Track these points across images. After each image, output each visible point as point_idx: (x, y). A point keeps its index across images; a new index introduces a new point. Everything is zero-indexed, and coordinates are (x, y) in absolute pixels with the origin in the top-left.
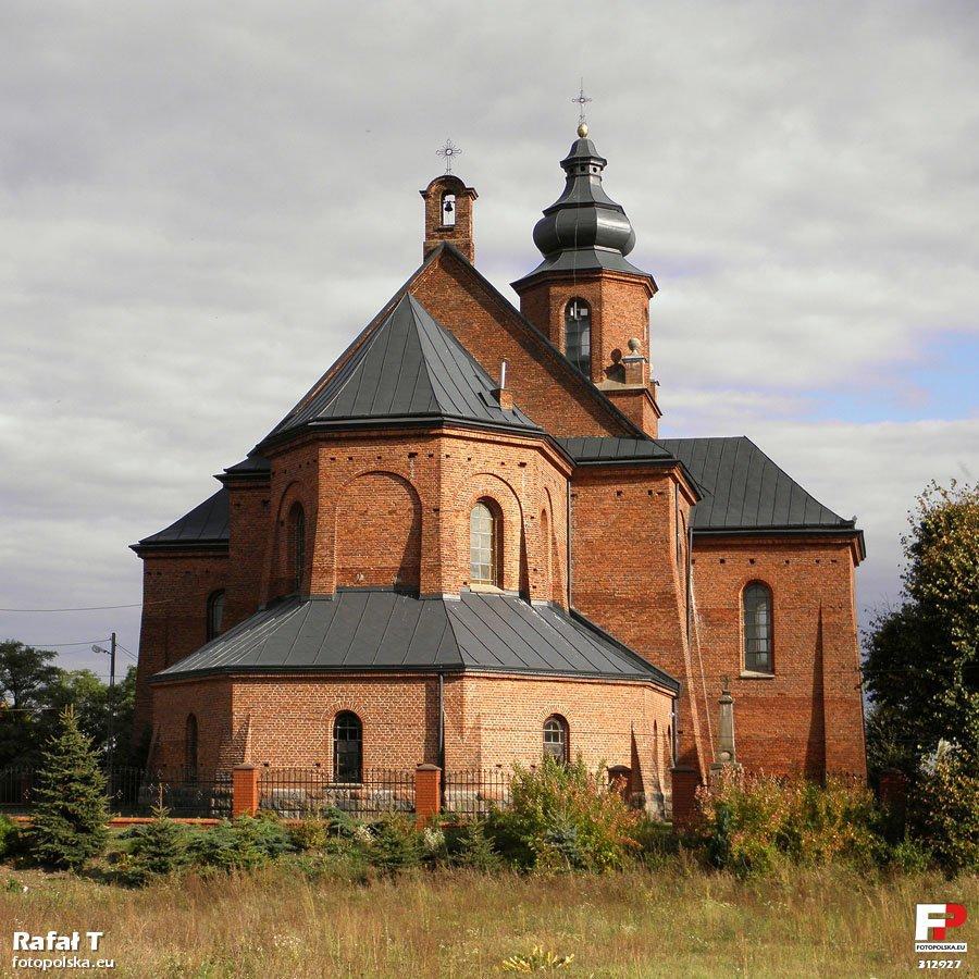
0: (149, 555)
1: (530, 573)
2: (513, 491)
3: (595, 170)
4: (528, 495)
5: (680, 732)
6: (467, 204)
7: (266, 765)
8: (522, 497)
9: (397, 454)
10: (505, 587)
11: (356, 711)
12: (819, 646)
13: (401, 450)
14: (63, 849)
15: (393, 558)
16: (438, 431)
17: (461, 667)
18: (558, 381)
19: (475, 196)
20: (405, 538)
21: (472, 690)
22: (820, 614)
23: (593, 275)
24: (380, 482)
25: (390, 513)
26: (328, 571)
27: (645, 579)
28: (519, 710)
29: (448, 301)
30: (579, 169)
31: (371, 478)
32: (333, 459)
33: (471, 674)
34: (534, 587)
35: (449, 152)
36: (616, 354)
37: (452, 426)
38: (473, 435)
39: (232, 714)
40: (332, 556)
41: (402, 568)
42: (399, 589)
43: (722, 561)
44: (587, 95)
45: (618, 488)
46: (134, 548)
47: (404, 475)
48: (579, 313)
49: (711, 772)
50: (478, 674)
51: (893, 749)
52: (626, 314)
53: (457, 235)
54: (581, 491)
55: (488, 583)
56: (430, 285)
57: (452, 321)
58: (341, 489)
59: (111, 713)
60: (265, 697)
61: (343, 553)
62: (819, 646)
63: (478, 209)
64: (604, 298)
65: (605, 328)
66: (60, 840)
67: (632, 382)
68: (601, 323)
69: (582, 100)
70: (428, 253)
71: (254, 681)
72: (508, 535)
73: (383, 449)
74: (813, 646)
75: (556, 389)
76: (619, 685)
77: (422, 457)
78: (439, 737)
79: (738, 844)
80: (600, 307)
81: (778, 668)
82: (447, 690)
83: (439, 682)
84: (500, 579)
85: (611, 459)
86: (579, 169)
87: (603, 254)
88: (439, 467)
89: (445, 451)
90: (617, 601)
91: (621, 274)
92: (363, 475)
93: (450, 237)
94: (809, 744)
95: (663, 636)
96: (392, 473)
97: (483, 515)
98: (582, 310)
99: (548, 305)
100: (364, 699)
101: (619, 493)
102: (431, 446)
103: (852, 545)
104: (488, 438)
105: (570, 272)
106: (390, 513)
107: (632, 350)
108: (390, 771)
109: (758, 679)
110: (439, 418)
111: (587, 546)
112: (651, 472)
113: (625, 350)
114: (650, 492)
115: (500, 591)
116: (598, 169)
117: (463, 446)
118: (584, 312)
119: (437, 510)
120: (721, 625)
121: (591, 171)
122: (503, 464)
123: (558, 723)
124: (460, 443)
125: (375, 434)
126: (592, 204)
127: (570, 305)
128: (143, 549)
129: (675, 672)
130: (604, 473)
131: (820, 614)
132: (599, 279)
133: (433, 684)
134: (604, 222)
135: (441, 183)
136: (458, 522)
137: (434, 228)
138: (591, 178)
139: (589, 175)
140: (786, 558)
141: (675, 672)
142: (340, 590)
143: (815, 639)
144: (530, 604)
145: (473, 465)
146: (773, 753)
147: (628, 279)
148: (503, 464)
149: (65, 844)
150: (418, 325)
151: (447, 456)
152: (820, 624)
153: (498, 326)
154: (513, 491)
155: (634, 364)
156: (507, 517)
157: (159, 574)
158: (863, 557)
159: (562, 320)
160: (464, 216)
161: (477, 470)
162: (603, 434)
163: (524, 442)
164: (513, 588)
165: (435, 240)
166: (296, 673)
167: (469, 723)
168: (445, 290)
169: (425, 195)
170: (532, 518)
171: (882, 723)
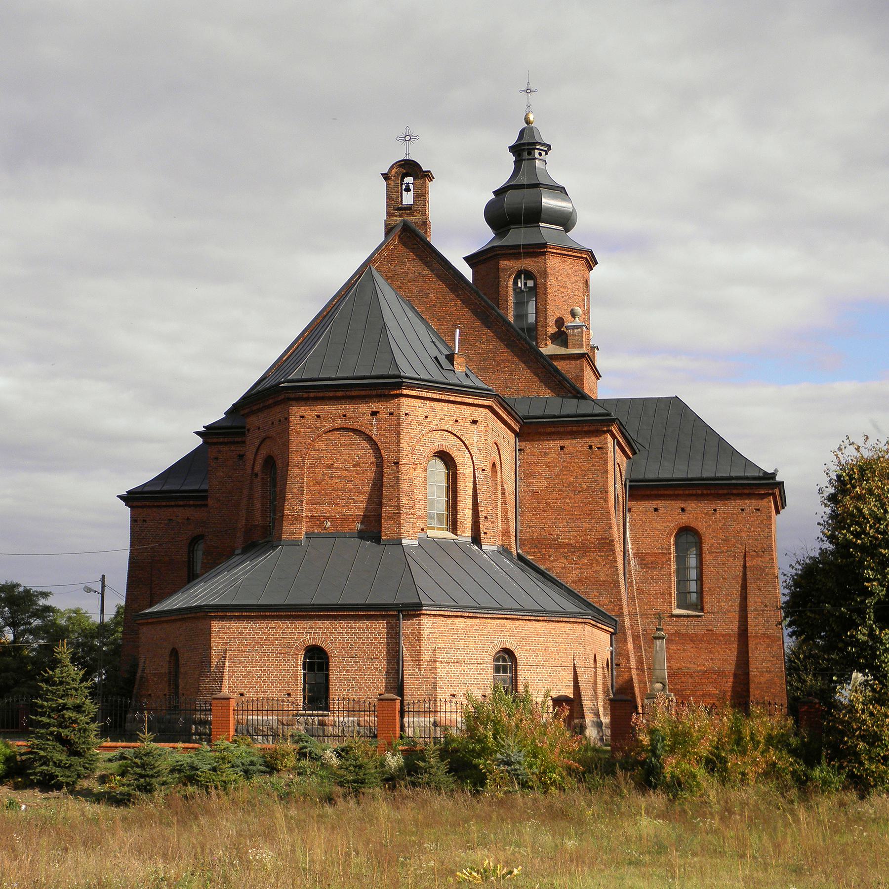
0: (135, 504)
1: (482, 521)
3: (540, 154)
5: (618, 665)
7: (242, 695)
8: (474, 451)
10: (459, 533)
12: (744, 587)
13: (365, 408)
14: (57, 771)
15: (357, 507)
16: (398, 392)
17: (419, 606)
18: (507, 346)
20: (367, 489)
21: (428, 625)
22: (745, 558)
23: (538, 250)
25: (354, 466)
26: (298, 519)
27: (586, 526)
29: (407, 273)
31: (337, 434)
32: (302, 417)
33: (428, 612)
34: (485, 533)
35: (408, 138)
36: (560, 322)
37: (411, 387)
38: (430, 395)
40: (301, 505)
41: (365, 516)
42: (362, 535)
43: (656, 510)
45: (562, 443)
47: (367, 432)
48: (525, 284)
49: (646, 701)
51: (811, 681)
52: (568, 285)
54: (532, 448)
56: (390, 259)
57: (410, 291)
60: (241, 633)
62: (744, 587)
63: (435, 191)
64: (549, 271)
66: (55, 763)
67: (574, 346)
69: (528, 91)
70: (389, 230)
71: (231, 618)
72: (461, 485)
73: (349, 408)
74: (738, 587)
75: (504, 353)
76: (562, 622)
77: (384, 415)
79: (671, 766)
81: (707, 606)
82: (406, 627)
84: (454, 527)
85: (555, 417)
86: (525, 154)
87: (548, 231)
88: (399, 424)
89: (404, 409)
90: (560, 546)
92: (330, 431)
93: (408, 215)
94: (735, 675)
95: (602, 578)
96: (356, 430)
97: (439, 469)
99: (497, 277)
101: (562, 448)
102: (391, 405)
103: (774, 495)
104: (443, 397)
106: (354, 466)
107: (575, 318)
109: (688, 616)
111: (533, 495)
112: (575, 429)
114: (590, 447)
115: (454, 536)
116: (543, 153)
119: (397, 463)
120: (655, 568)
121: (537, 155)
122: (457, 421)
123: (506, 656)
124: (418, 403)
125: (340, 394)
127: (518, 277)
128: (130, 498)
129: (613, 610)
130: (549, 430)
131: (745, 558)
132: (544, 253)
133: (393, 621)
134: (548, 202)
135: (400, 166)
136: (415, 474)
137: (394, 207)
138: (537, 161)
139: (535, 159)
140: (714, 506)
141: (613, 610)
142: (309, 536)
143: (740, 581)
144: (481, 548)
145: (430, 423)
146: (702, 684)
147: (570, 253)
149: (59, 766)
151: (406, 414)
152: (745, 567)
153: (452, 296)
155: (575, 331)
156: (461, 470)
158: (784, 505)
160: (421, 196)
162: (547, 394)
163: (476, 402)
164: (466, 534)
165: (395, 218)
166: (385, 611)
167: (426, 656)
168: (404, 263)
169: (386, 177)
170: (483, 470)
171: (801, 656)
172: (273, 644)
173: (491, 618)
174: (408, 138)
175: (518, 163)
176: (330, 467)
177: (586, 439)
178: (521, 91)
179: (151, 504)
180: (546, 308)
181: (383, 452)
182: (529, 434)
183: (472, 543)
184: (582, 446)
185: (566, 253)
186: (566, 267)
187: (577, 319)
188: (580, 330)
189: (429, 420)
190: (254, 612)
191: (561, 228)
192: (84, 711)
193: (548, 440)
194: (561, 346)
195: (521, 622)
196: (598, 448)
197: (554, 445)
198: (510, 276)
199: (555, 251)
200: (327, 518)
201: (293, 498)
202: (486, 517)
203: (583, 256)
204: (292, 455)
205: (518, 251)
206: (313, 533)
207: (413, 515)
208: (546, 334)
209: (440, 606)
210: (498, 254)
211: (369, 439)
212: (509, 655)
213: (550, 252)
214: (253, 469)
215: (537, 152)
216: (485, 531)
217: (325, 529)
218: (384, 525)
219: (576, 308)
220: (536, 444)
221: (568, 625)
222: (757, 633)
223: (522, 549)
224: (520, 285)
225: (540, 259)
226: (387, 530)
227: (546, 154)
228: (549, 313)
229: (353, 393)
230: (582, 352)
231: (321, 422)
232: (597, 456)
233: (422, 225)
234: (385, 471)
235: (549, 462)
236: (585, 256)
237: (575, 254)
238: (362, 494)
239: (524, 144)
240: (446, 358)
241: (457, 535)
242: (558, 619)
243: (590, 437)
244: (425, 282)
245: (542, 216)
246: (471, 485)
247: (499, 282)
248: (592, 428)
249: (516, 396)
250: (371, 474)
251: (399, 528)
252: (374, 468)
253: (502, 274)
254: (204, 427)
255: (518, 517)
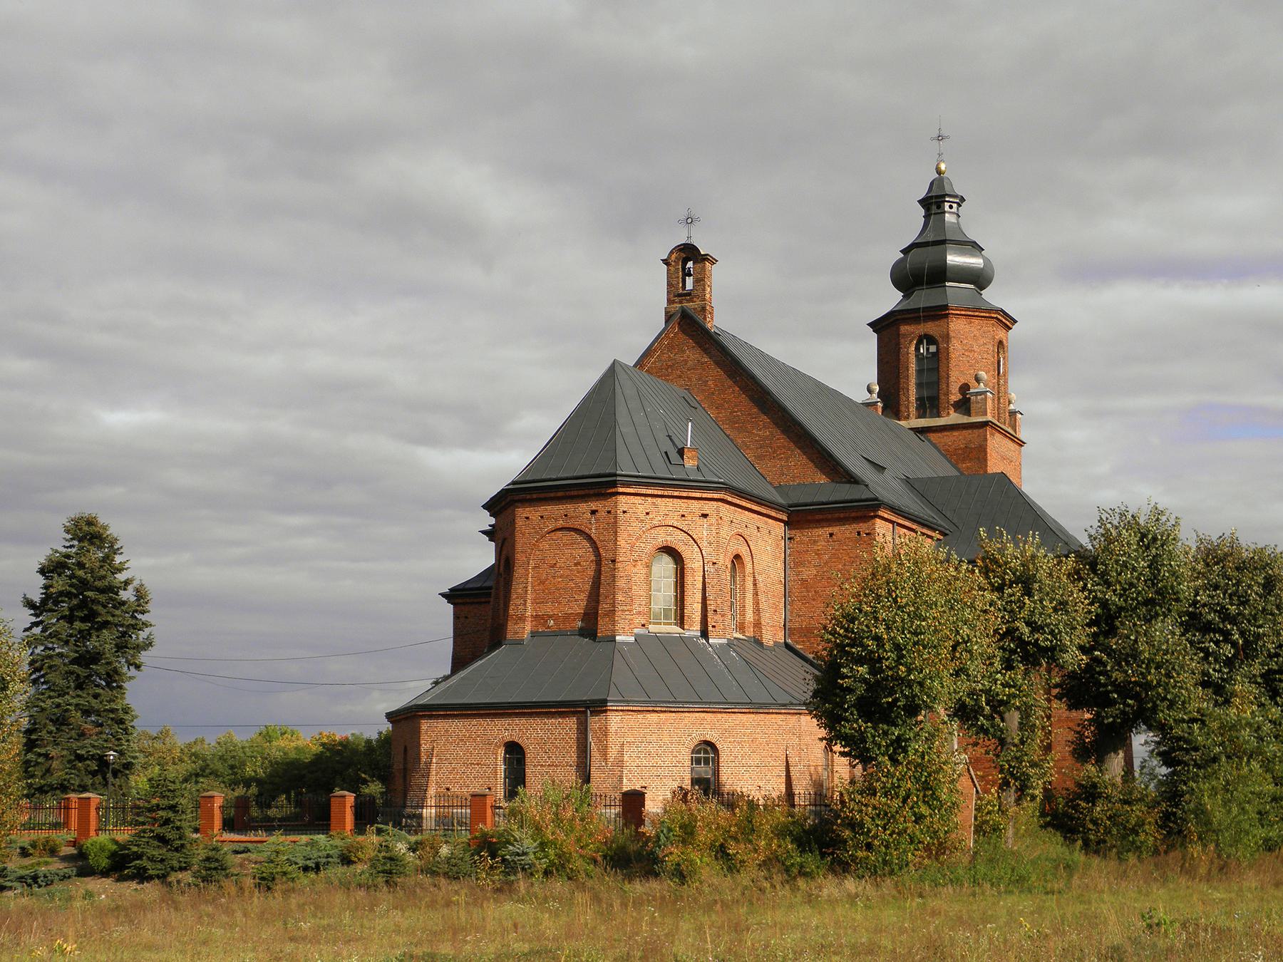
0: (457, 601)
1: (710, 614)
2: (694, 540)
3: (951, 207)
4: (710, 543)
6: (704, 268)
7: (448, 789)
8: (704, 544)
9: (581, 511)
10: (686, 627)
11: (520, 742)
13: (584, 508)
14: (148, 865)
15: (578, 605)
16: (614, 490)
17: (604, 702)
18: (784, 432)
19: (713, 261)
20: (588, 587)
21: (615, 721)
23: (939, 313)
24: (567, 537)
25: (576, 565)
26: (522, 619)
28: (666, 739)
29: (686, 361)
30: (934, 207)
31: (559, 534)
32: (527, 518)
33: (614, 708)
34: (714, 627)
35: (690, 221)
36: (965, 388)
37: (628, 485)
38: (650, 492)
39: (420, 745)
40: (525, 605)
41: (585, 614)
42: (583, 633)
44: (944, 133)
45: (830, 530)
46: (443, 595)
47: (587, 531)
48: (928, 349)
50: (620, 708)
52: (976, 348)
53: (695, 299)
54: (801, 536)
55: (670, 624)
56: (670, 347)
57: (690, 379)
58: (534, 545)
59: (1114, 721)
60: (447, 731)
61: (535, 602)
63: (717, 275)
64: (952, 334)
65: (953, 363)
66: (149, 858)
67: (977, 414)
68: (948, 359)
69: (940, 138)
70: (669, 317)
71: (438, 717)
72: (689, 580)
73: (569, 508)
75: (781, 440)
76: (772, 713)
77: (602, 514)
78: (586, 764)
79: (673, 854)
80: (948, 343)
82: (594, 722)
83: (587, 716)
84: (681, 621)
85: (823, 504)
86: (934, 207)
87: (955, 291)
88: (616, 522)
89: (622, 507)
91: (968, 309)
92: (552, 531)
93: (688, 301)
96: (578, 530)
97: (665, 566)
98: (931, 347)
99: (898, 344)
100: (528, 731)
101: (831, 535)
102: (609, 503)
104: (666, 493)
105: (917, 310)
106: (576, 565)
107: (979, 384)
108: (596, 795)
110: (614, 478)
111: (802, 584)
112: (842, 515)
113: (973, 382)
114: (859, 533)
115: (680, 630)
116: (955, 206)
117: (640, 501)
118: (933, 349)
119: (614, 561)
121: (947, 208)
122: (683, 516)
123: (709, 748)
124: (638, 500)
125: (560, 494)
126: (943, 242)
127: (920, 342)
128: (454, 596)
130: (817, 517)
132: (946, 316)
133: (583, 718)
134: (953, 259)
135: (680, 250)
136: (635, 570)
137: (676, 294)
138: (947, 215)
142: (534, 634)
144: (708, 642)
145: (652, 519)
147: (977, 314)
148: (683, 516)
149: (151, 861)
150: (618, 390)
151: (624, 512)
153: (730, 382)
154: (694, 540)
155: (979, 397)
156: (689, 565)
157: (466, 617)
159: (913, 359)
160: (700, 281)
161: (657, 523)
162: (822, 479)
163: (705, 495)
164: (694, 630)
165: (675, 305)
166: (574, 707)
167: (613, 752)
168: (684, 352)
169: (666, 262)
170: (714, 563)
172: (475, 740)
173: (688, 712)
174: (689, 221)
175: (927, 217)
176: (553, 567)
177: (854, 526)
178: (932, 139)
179: (472, 600)
180: (948, 374)
181: (601, 550)
182: (798, 521)
183: (701, 636)
184: (851, 532)
185: (972, 313)
186: (973, 329)
187: (982, 384)
188: (983, 396)
189: (651, 516)
190: (457, 711)
191: (972, 286)
192: (178, 811)
193: (817, 528)
194: (964, 414)
195: (724, 715)
196: (866, 534)
197: (823, 532)
198: (911, 341)
199: (958, 312)
200: (550, 617)
201: (517, 598)
202: (715, 611)
203: (993, 315)
204: (518, 556)
205: (916, 315)
206: (538, 632)
207: (630, 611)
208: (948, 402)
209: (627, 701)
210: (897, 320)
211: (589, 538)
212: (711, 747)
213: (953, 314)
214: (499, 570)
215: (947, 205)
216: (714, 624)
217: (549, 627)
218: (600, 622)
219: (981, 373)
220: (805, 532)
221: (780, 716)
222: (1060, 716)
223: (791, 639)
224: (922, 351)
225: (942, 322)
226: (603, 628)
227: (959, 205)
228: (952, 379)
229: (573, 493)
230: (984, 420)
231: (544, 523)
232: (865, 542)
233: (701, 311)
234: (603, 569)
235: (818, 550)
236: (995, 316)
237: (982, 314)
238: (583, 592)
239: (931, 197)
240: (678, 452)
241: (684, 629)
242: (777, 711)
243: (858, 523)
244: (704, 370)
245: (948, 274)
246: (701, 579)
247: (900, 348)
248: (859, 514)
249: (791, 483)
250: (591, 573)
251: (614, 625)
252: (593, 566)
253: (902, 341)
254: (490, 526)
255: (788, 607)
